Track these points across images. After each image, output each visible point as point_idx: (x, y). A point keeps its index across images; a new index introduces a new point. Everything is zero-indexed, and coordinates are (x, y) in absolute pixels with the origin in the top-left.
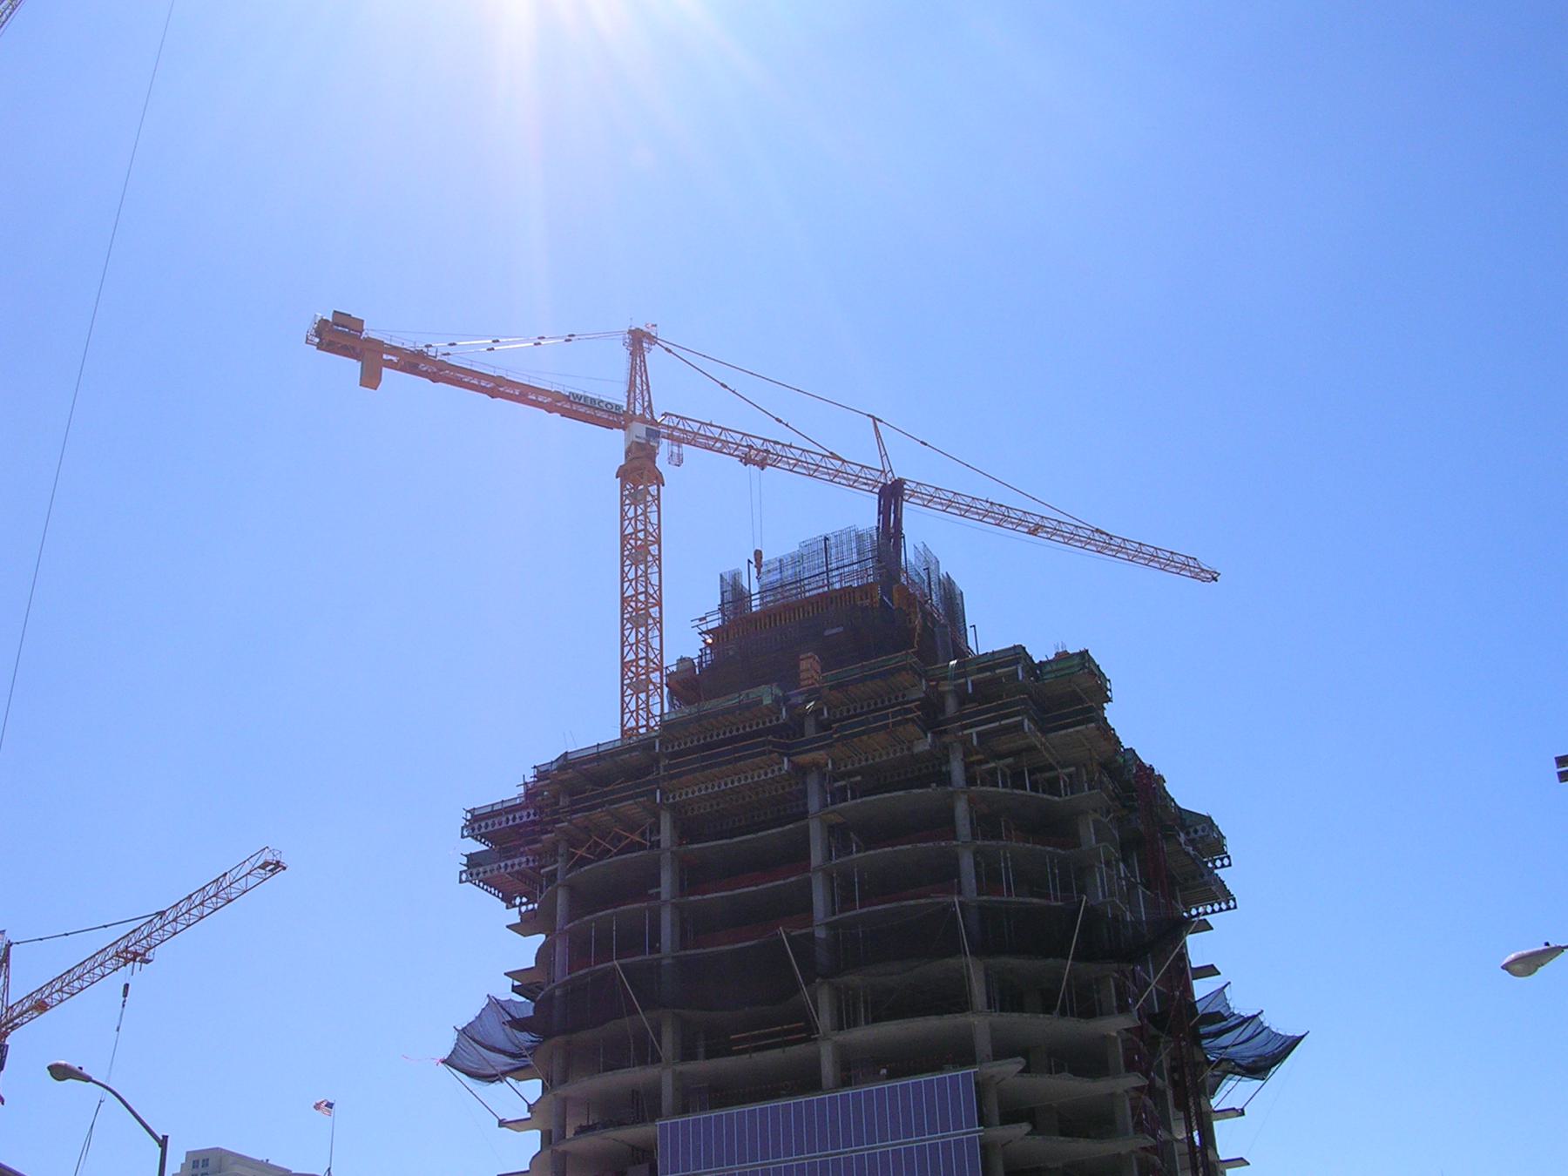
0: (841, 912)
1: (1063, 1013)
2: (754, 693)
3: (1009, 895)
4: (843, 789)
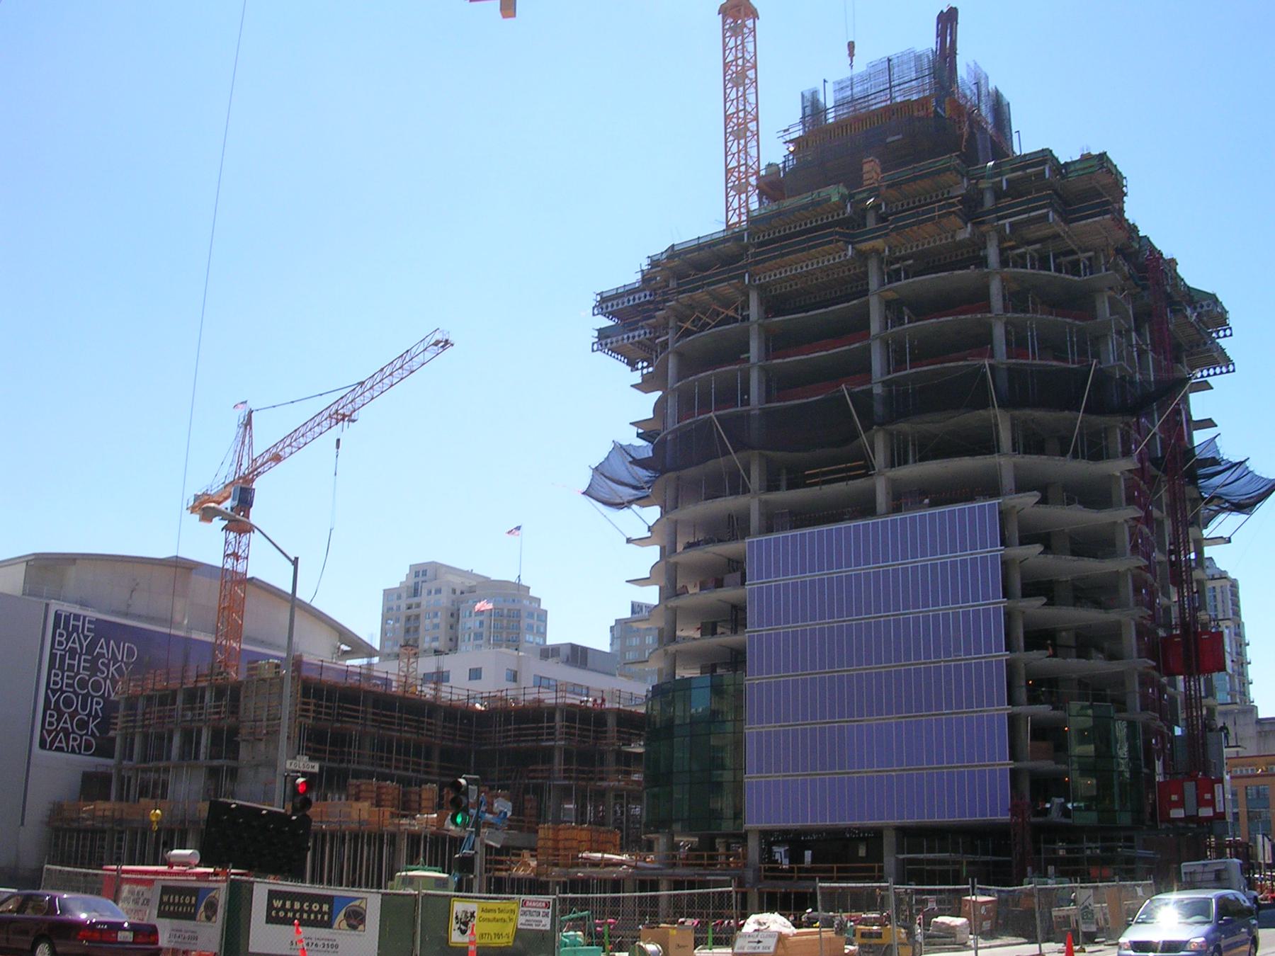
0: (895, 371)
1: (1075, 456)
2: (824, 192)
3: (1034, 358)
4: (898, 271)
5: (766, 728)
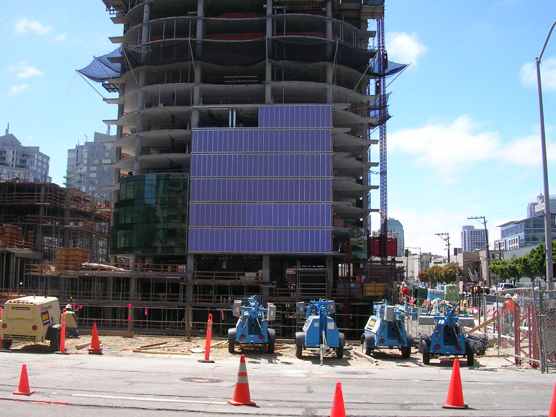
5: (201, 202)
